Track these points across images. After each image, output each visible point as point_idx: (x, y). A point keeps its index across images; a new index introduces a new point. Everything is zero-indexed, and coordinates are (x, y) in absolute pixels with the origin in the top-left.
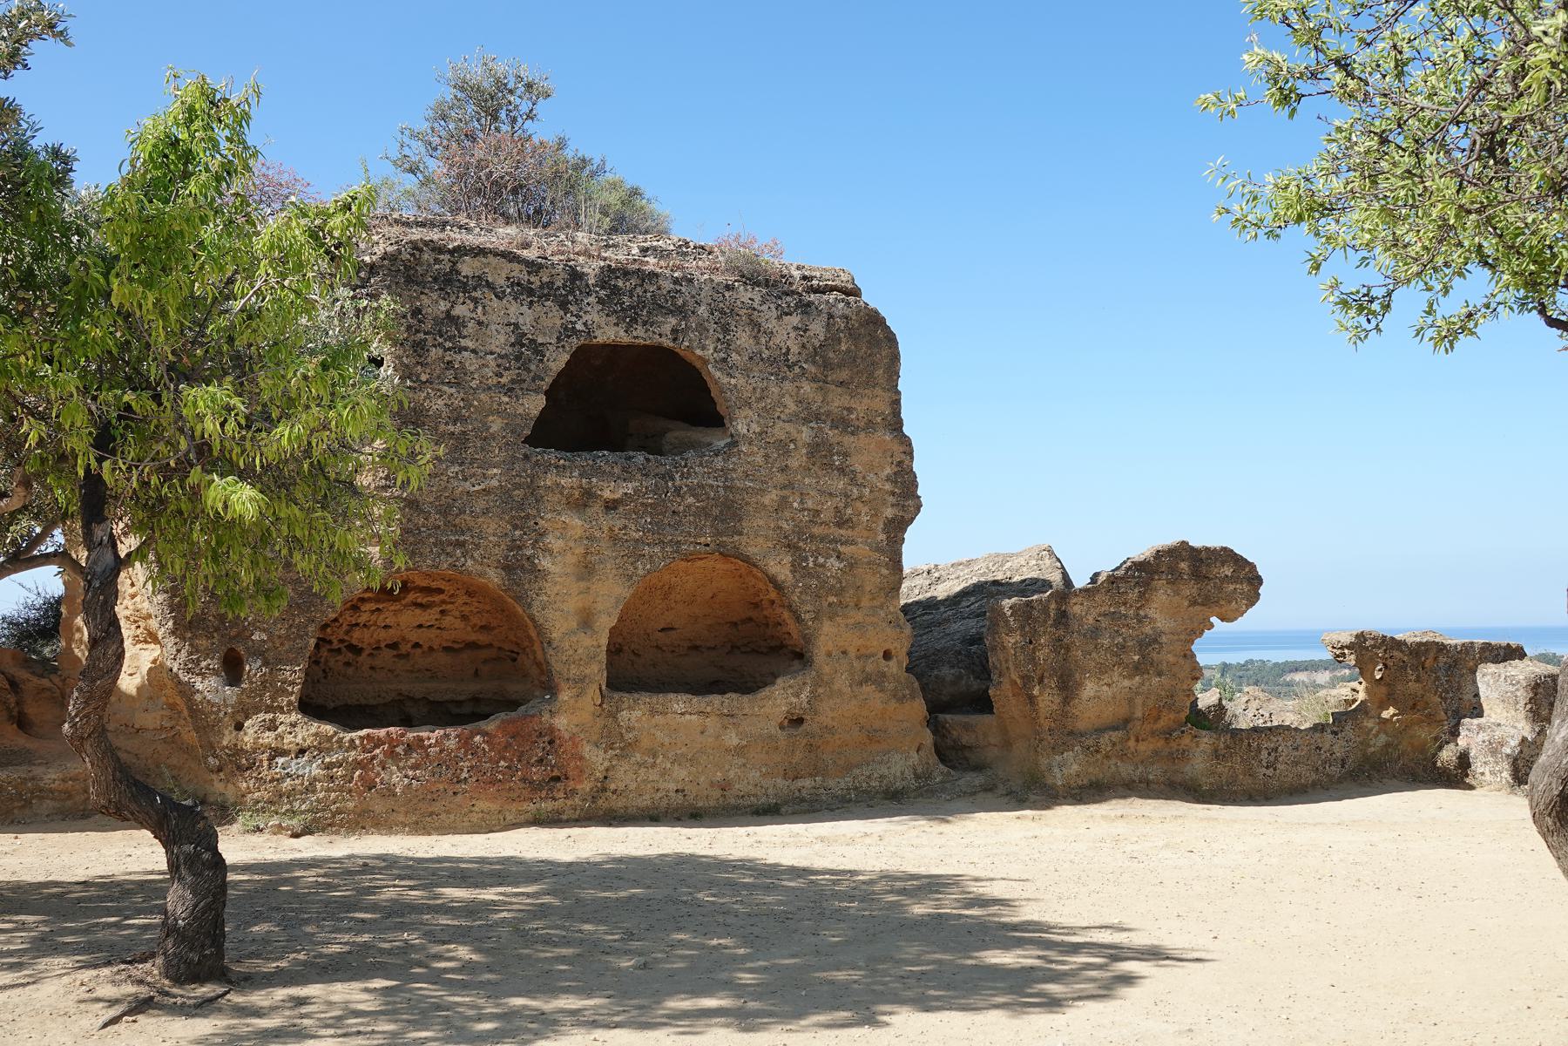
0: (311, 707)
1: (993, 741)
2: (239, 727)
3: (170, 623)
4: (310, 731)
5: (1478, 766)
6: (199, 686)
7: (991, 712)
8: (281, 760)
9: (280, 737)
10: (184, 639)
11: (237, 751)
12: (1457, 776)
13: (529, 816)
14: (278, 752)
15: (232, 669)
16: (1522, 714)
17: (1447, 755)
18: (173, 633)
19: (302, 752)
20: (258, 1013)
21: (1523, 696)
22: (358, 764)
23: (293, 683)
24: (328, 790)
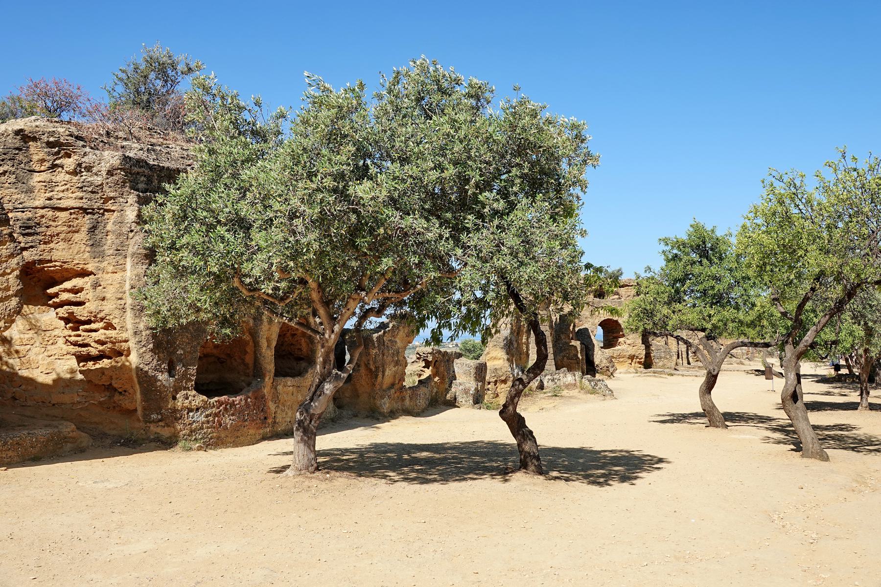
0: (200, 388)
1: (347, 395)
2: (174, 398)
3: (151, 346)
4: (200, 399)
5: (459, 399)
6: (160, 378)
7: (557, 369)
8: (191, 414)
9: (190, 402)
10: (155, 354)
11: (175, 410)
12: (452, 404)
13: (258, 437)
14: (190, 410)
15: (171, 371)
16: (473, 378)
17: (448, 397)
18: (151, 350)
19: (197, 409)
20: (95, 331)
21: (473, 371)
22: (216, 415)
23: (193, 375)
24: (208, 428)
